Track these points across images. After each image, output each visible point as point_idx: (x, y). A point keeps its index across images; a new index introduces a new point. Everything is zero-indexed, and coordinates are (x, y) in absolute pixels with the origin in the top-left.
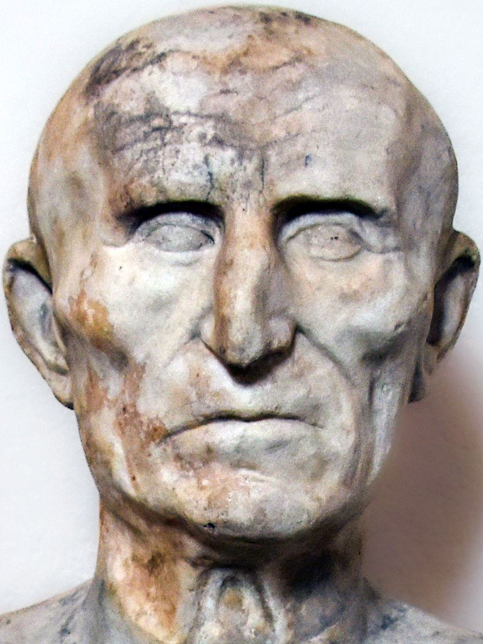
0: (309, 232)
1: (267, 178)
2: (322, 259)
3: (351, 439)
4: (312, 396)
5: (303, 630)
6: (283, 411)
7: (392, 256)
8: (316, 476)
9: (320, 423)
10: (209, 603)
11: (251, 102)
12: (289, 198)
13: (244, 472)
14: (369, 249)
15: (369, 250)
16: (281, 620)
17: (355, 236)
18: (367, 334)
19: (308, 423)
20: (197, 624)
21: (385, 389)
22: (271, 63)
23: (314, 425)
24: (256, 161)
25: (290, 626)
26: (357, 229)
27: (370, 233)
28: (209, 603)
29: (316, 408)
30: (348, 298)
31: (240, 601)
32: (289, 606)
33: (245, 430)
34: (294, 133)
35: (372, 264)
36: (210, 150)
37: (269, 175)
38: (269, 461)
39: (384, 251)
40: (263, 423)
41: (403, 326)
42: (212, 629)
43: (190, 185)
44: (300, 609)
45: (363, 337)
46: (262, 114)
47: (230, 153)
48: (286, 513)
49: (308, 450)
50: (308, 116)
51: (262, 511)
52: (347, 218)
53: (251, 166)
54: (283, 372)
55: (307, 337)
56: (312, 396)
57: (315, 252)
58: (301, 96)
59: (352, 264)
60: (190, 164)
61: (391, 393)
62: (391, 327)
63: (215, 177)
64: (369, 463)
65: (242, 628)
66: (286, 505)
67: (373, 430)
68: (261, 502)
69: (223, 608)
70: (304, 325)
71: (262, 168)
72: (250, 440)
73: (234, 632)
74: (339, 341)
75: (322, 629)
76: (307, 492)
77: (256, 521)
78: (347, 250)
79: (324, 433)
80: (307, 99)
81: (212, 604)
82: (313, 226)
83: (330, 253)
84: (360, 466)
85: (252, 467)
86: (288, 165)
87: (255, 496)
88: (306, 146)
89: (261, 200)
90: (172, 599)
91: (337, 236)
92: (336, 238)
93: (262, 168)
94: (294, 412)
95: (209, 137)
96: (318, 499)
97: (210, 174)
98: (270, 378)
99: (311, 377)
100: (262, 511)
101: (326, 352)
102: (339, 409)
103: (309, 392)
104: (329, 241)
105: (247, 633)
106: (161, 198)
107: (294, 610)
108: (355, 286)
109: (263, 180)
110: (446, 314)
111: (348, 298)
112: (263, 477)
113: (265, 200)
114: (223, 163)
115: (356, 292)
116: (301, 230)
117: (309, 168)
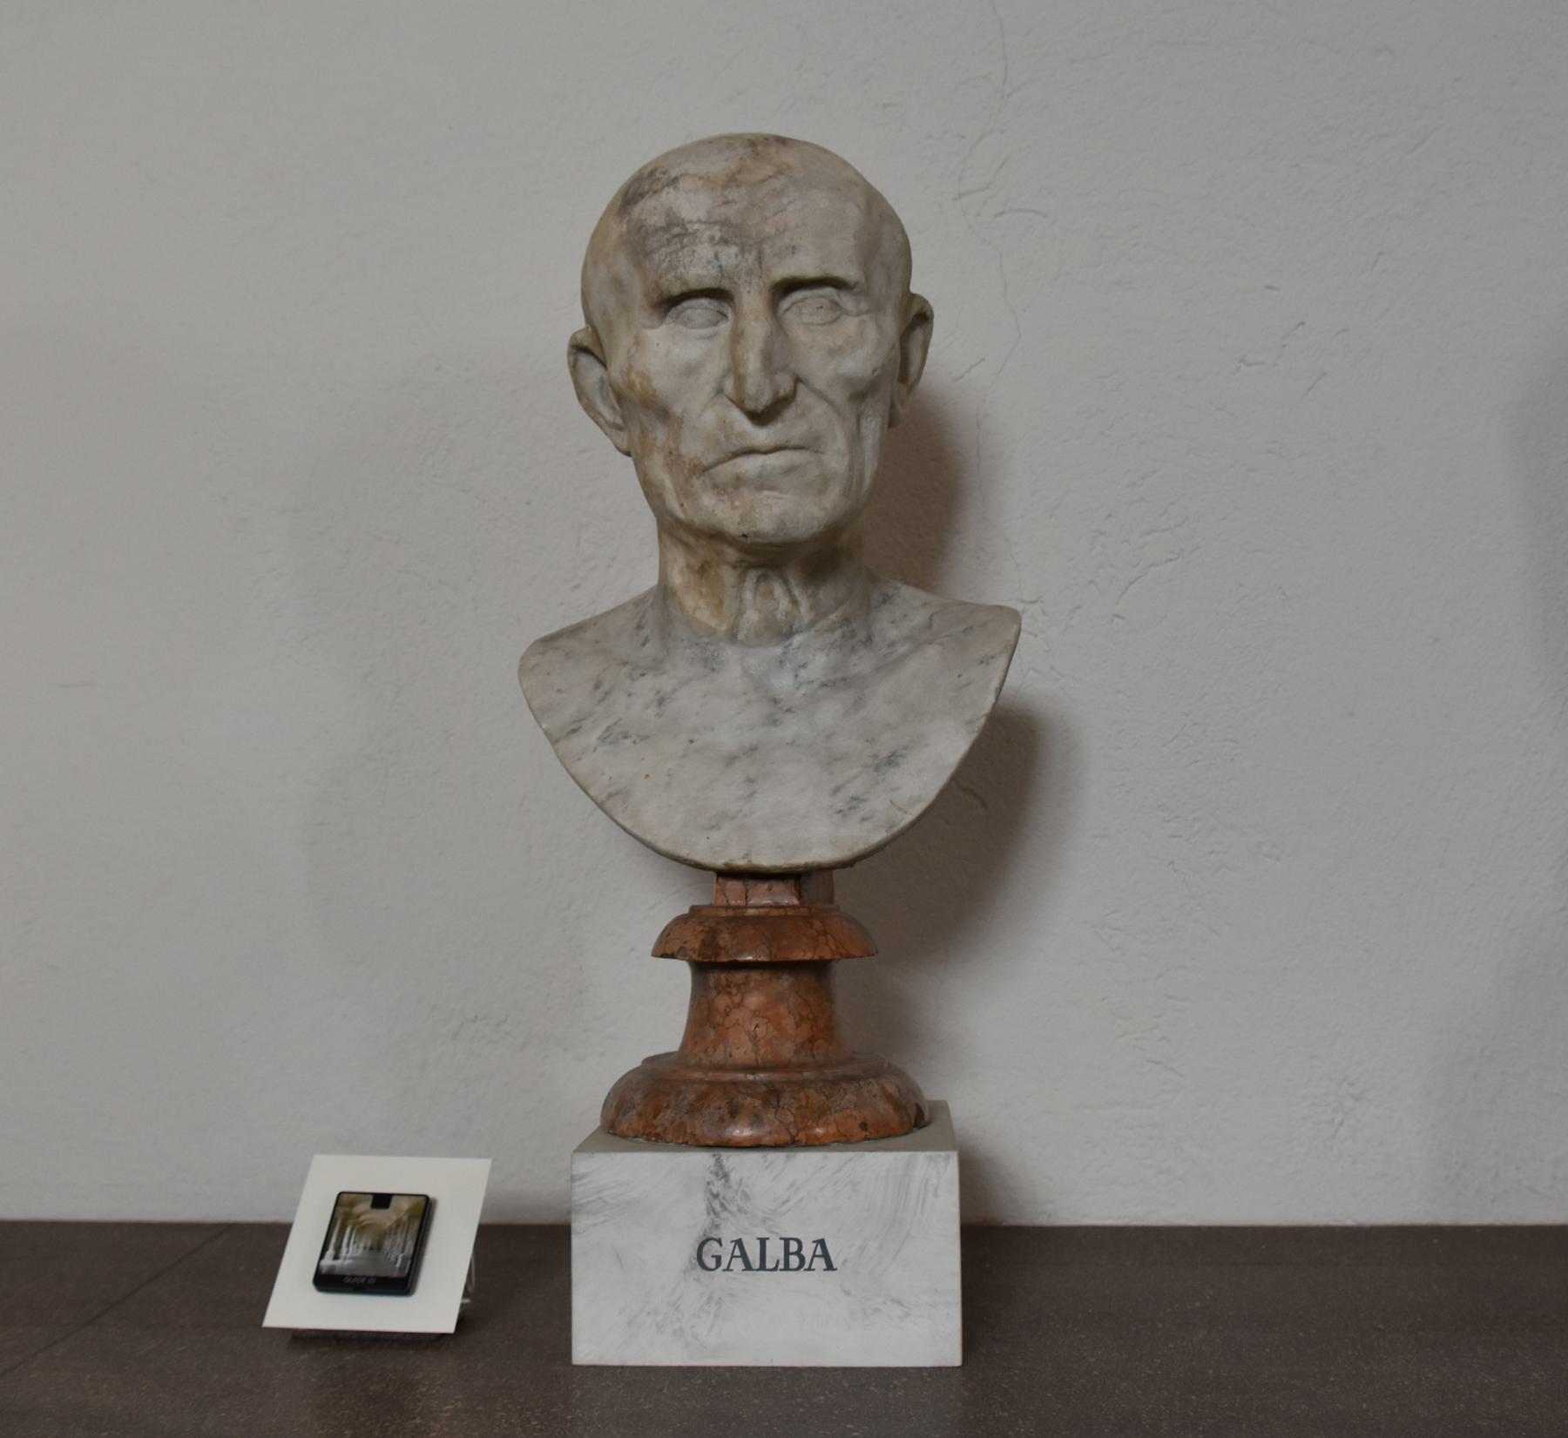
0: (800, 304)
1: (764, 266)
2: (812, 324)
3: (846, 460)
4: (813, 430)
6: (793, 443)
7: (865, 317)
8: (822, 491)
10: (748, 596)
13: (766, 493)
14: (847, 313)
15: (847, 314)
17: (835, 305)
20: (740, 613)
23: (817, 452)
24: (754, 253)
25: (812, 608)
27: (847, 301)
28: (748, 596)
30: (834, 352)
31: (771, 592)
33: (764, 461)
35: (850, 325)
36: (717, 248)
39: (859, 314)
40: (777, 454)
45: (848, 381)
47: (734, 250)
53: (751, 258)
54: (790, 414)
56: (813, 430)
57: (806, 319)
58: (785, 200)
61: (874, 423)
62: (869, 372)
63: (724, 268)
64: (861, 477)
71: (760, 259)
79: (825, 458)
80: (790, 203)
82: (802, 300)
83: (817, 319)
84: (855, 481)
85: (772, 489)
87: (776, 510)
89: (761, 283)
92: (822, 307)
93: (760, 259)
95: (717, 238)
96: (825, 509)
97: (720, 267)
101: (820, 395)
103: (811, 428)
109: (761, 267)
111: (834, 352)
113: (764, 283)
116: (794, 304)
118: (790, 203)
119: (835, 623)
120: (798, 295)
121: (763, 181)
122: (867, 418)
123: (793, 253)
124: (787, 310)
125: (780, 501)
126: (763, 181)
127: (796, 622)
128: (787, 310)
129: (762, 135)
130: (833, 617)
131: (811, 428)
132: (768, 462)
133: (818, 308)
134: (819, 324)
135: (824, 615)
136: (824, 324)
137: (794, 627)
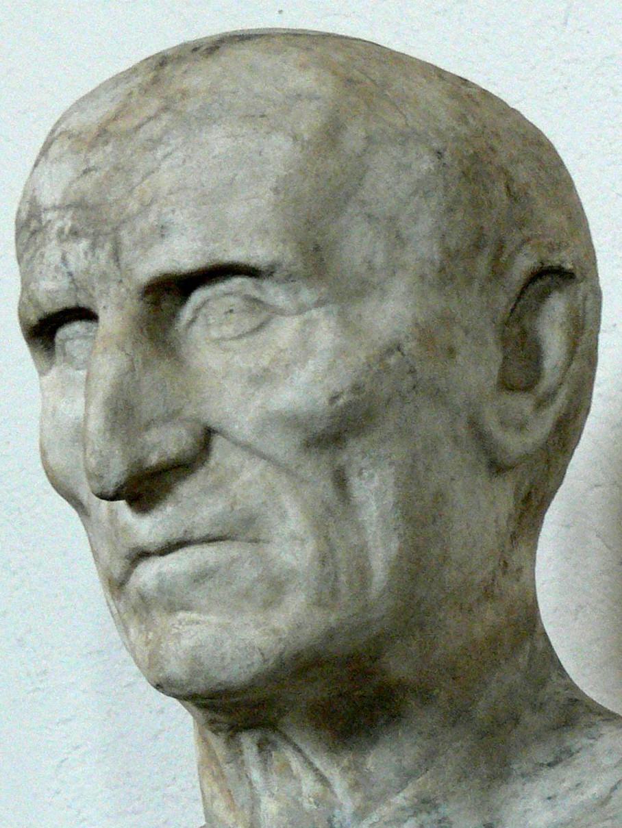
0: (204, 311)
1: (123, 265)
2: (223, 339)
3: (310, 547)
4: (238, 508)
5: (375, 791)
6: (197, 534)
7: (314, 313)
9: (262, 536)
10: (256, 775)
11: (108, 177)
12: (151, 281)
13: (181, 615)
14: (282, 312)
15: (282, 315)
16: (340, 784)
18: (296, 417)
19: (246, 541)
20: (255, 802)
21: (366, 474)
22: (136, 122)
23: (256, 541)
24: (108, 246)
25: (355, 786)
26: (256, 294)
27: (275, 294)
28: (256, 775)
29: (250, 521)
30: (261, 379)
31: (287, 765)
32: (345, 762)
33: (160, 567)
34: (147, 200)
35: (285, 331)
36: (67, 246)
37: (125, 256)
38: (199, 596)
39: (301, 310)
41: (345, 397)
42: (270, 807)
43: (57, 291)
44: (363, 764)
45: (291, 421)
46: (118, 191)
47: (84, 244)
48: (228, 657)
49: (248, 573)
50: (166, 178)
51: (195, 659)
52: (237, 282)
53: (103, 255)
54: (187, 489)
55: (224, 436)
56: (238, 508)
57: (215, 334)
58: (159, 153)
59: (261, 337)
60: (53, 267)
61: (376, 478)
62: (324, 401)
63: (75, 275)
65: (300, 799)
66: (228, 646)
67: (360, 528)
68: (193, 648)
69: (274, 777)
70: (214, 426)
71: (116, 255)
72: (168, 577)
73: (293, 806)
74: (261, 433)
75: (402, 787)
76: (258, 626)
77: (194, 673)
78: (248, 323)
79: (272, 550)
80: (165, 157)
81: (258, 776)
82: (204, 303)
83: (228, 330)
84: (343, 578)
85: (187, 608)
86: (144, 244)
87: (186, 643)
88: (160, 214)
89: (123, 290)
90: (444, 756)
91: (231, 308)
92: (231, 311)
93: (116, 255)
94: (216, 532)
95: (67, 230)
97: (70, 274)
98: (170, 497)
99: (235, 486)
100: (195, 659)
101: (249, 449)
102: (283, 516)
104: (224, 317)
105: (307, 806)
106: (41, 315)
107: (356, 767)
108: (265, 362)
109: (119, 266)
110: (544, 347)
111: (261, 379)
112: (202, 618)
113: (128, 290)
114: (78, 258)
115: (266, 370)
116: (197, 310)
117: (166, 241)
118: (165, 157)
119: (403, 809)
120: (198, 296)
121: (139, 127)
122: (360, 474)
123: (163, 236)
124: (193, 321)
125: (195, 628)
126: (139, 127)
127: (337, 811)
128: (193, 321)
129: (185, 45)
130: (399, 800)
131: (235, 503)
132: (164, 569)
133: (226, 313)
134: (233, 339)
135: (382, 798)
136: (240, 337)
137: (335, 820)
